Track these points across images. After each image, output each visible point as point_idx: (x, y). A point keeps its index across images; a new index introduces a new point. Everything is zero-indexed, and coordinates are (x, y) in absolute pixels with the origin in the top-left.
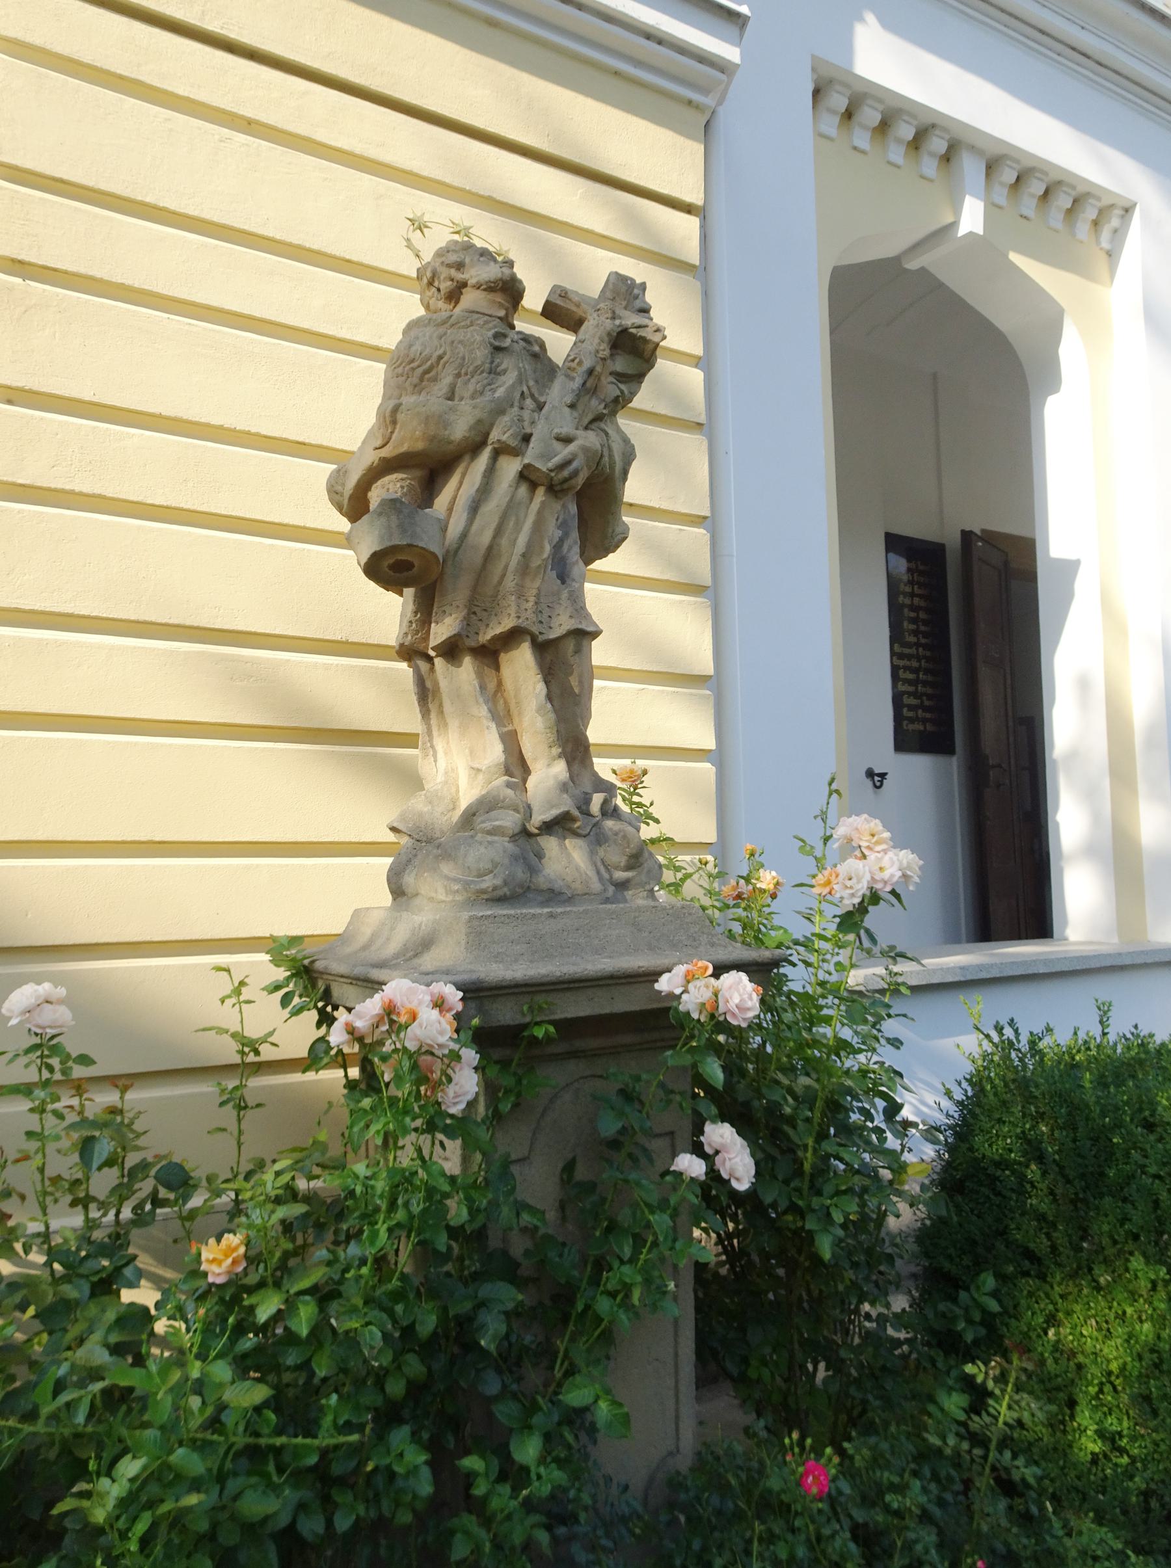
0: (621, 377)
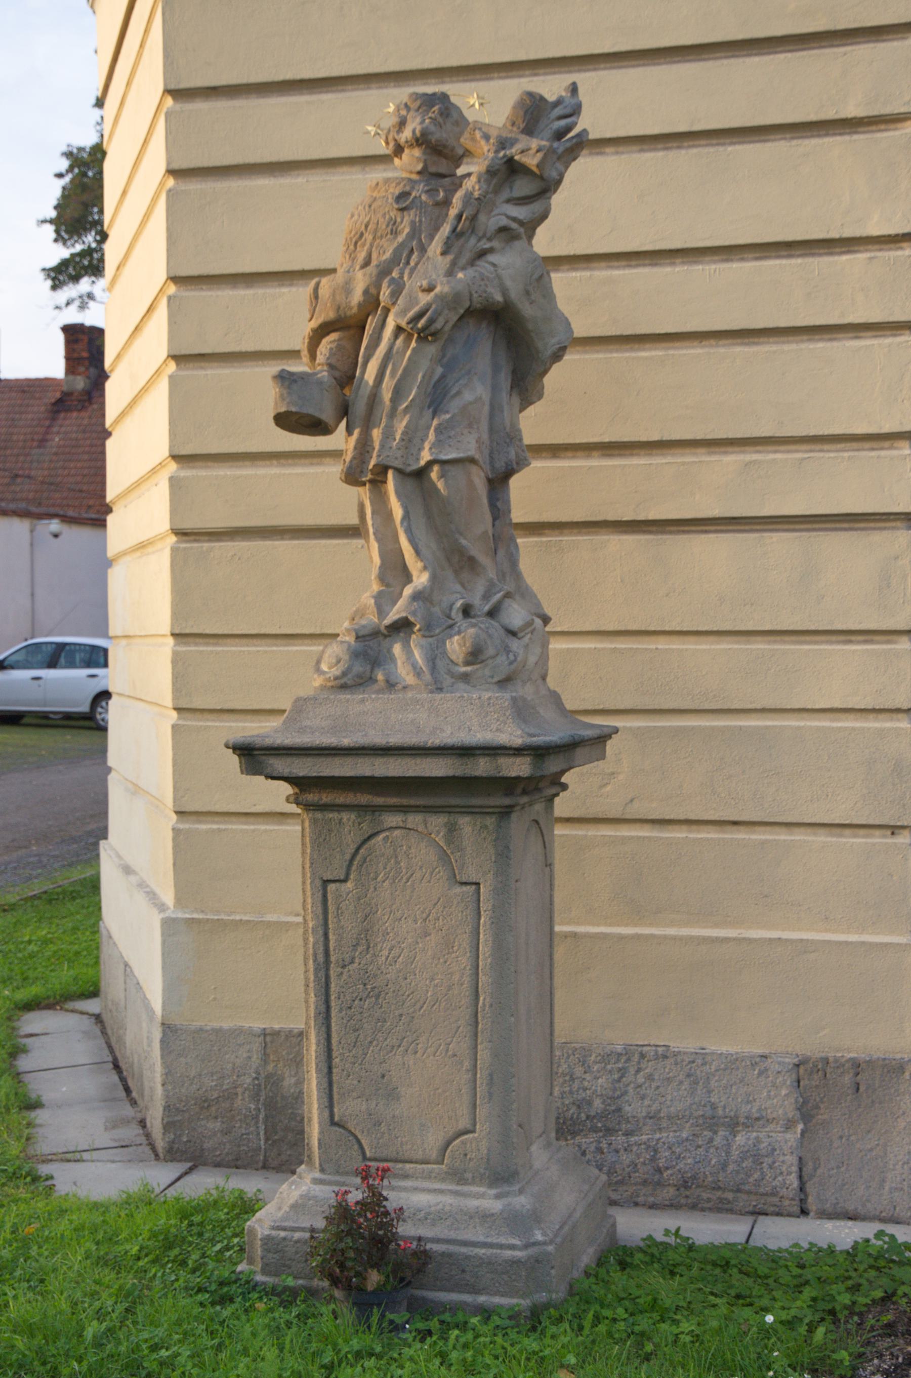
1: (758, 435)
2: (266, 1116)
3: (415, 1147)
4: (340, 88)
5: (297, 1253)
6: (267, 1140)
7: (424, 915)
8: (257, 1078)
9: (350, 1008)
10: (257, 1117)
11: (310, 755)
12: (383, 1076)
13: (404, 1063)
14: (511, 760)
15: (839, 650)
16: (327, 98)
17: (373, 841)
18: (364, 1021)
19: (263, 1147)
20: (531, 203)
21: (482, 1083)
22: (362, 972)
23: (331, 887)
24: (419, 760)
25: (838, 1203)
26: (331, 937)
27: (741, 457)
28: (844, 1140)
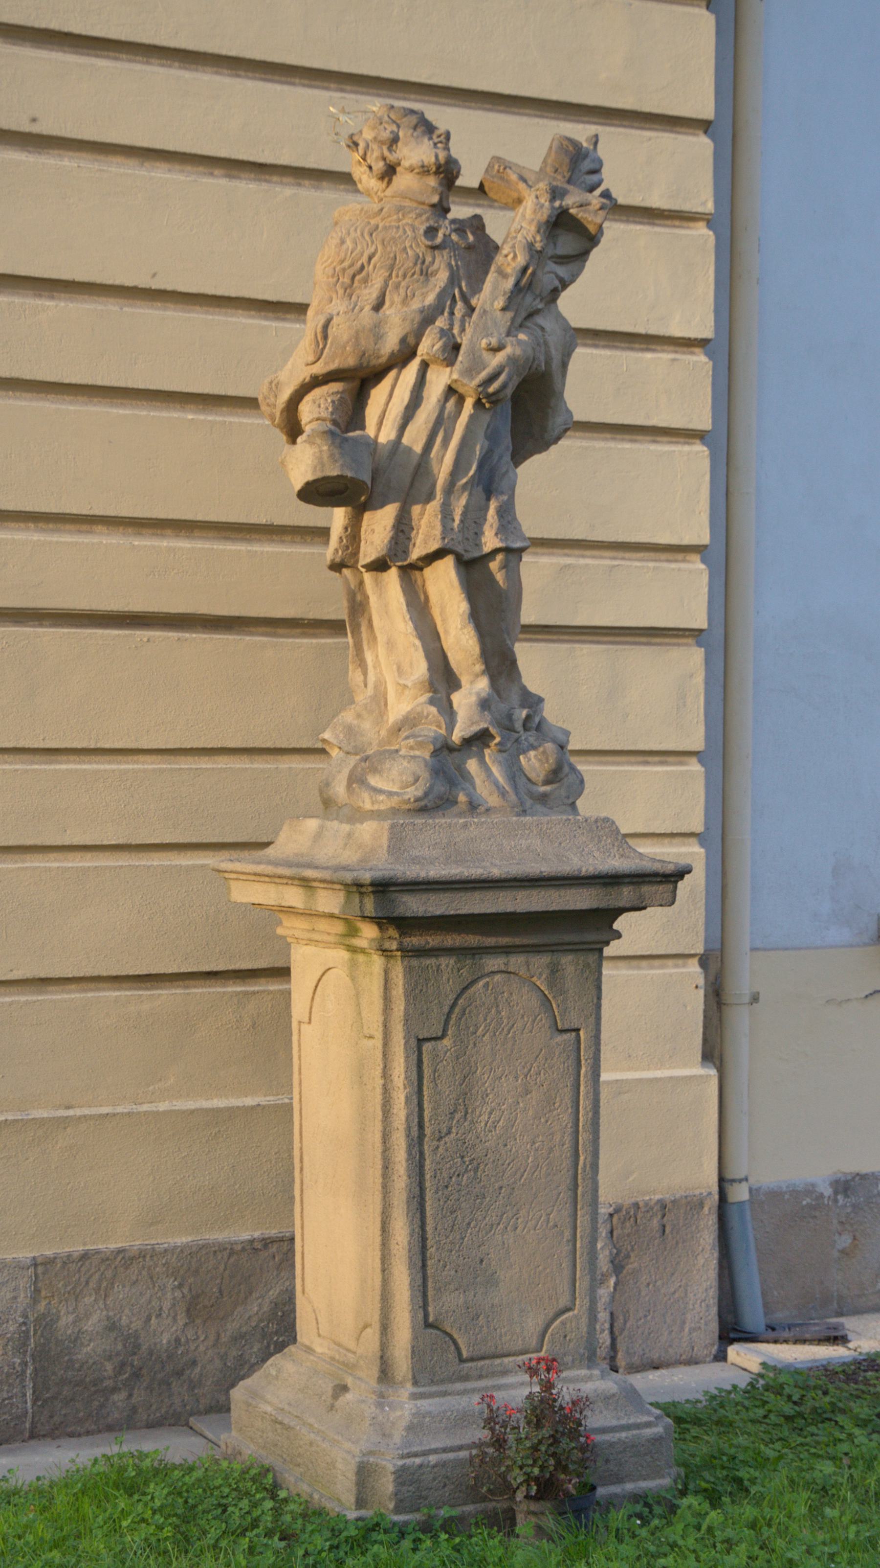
0: (562, 260)
1: (571, 537)
2: (35, 1369)
3: (515, 1337)
4: (111, 54)
5: (434, 1479)
6: (34, 1402)
7: (526, 1070)
8: (24, 1323)
9: (447, 1187)
10: (24, 1372)
11: (448, 889)
12: (482, 1261)
13: (503, 1243)
14: (654, 888)
15: (643, 772)
16: (102, 64)
17: (472, 990)
18: (462, 1199)
19: (31, 1411)
20: (567, 263)
21: (583, 1253)
22: (460, 1143)
23: (427, 1047)
24: (562, 892)
25: (644, 1354)
26: (426, 1105)
27: (554, 560)
28: (651, 1286)
